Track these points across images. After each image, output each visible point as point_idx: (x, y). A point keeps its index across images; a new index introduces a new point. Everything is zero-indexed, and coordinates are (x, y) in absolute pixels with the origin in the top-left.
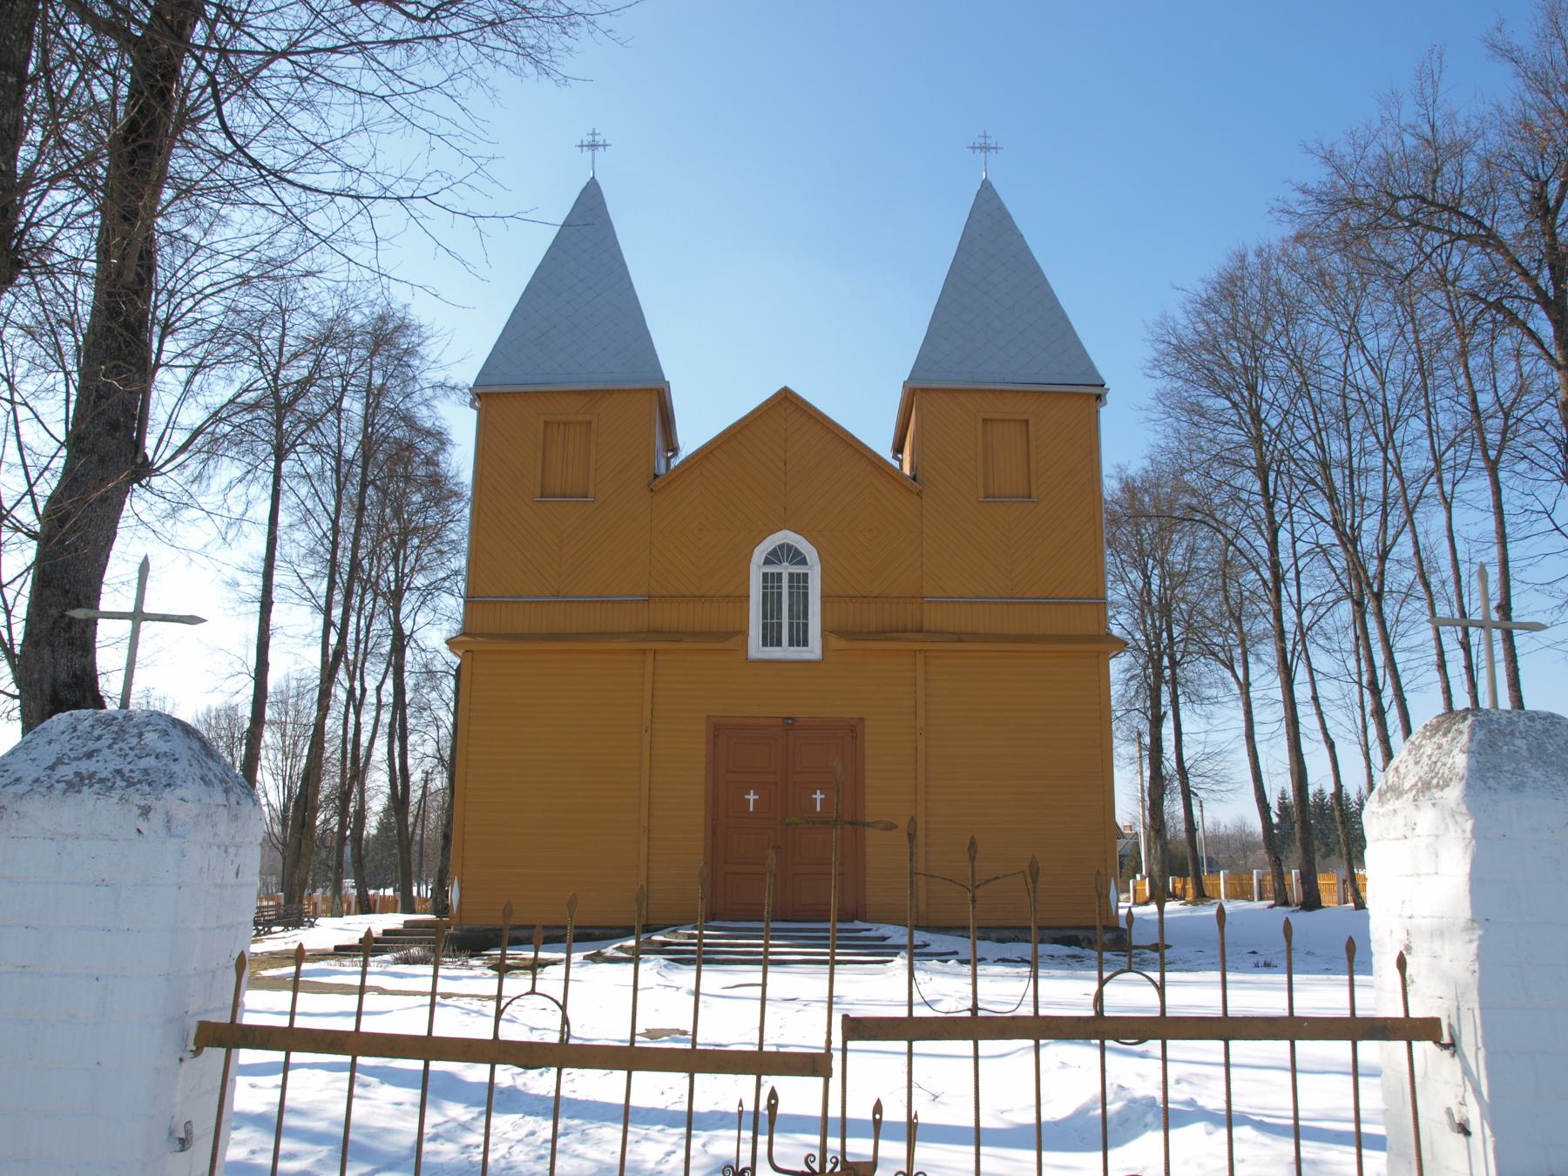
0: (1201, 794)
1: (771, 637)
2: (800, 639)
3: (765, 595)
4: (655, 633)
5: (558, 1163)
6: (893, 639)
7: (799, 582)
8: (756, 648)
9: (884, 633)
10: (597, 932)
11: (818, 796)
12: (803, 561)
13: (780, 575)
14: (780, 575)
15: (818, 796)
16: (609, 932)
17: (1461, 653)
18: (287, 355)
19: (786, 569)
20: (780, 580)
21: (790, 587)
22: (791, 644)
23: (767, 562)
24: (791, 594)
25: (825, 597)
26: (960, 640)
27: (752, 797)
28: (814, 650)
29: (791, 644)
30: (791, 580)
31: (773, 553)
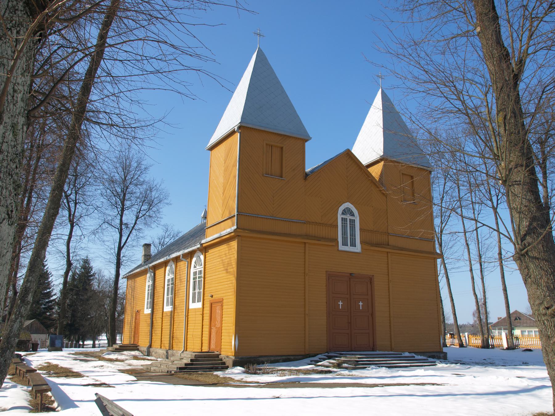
0: (114, 254)
1: (345, 244)
2: (353, 244)
3: (342, 226)
4: (308, 236)
5: (113, 272)
6: (384, 248)
7: (352, 222)
8: (341, 247)
9: (377, 245)
10: (292, 357)
11: (361, 304)
12: (353, 215)
13: (346, 219)
14: (346, 219)
15: (361, 304)
16: (296, 357)
17: (479, 265)
18: (116, 34)
19: (348, 217)
20: (347, 221)
21: (350, 224)
22: (351, 246)
23: (343, 214)
24: (350, 227)
25: (361, 229)
26: (402, 250)
27: (340, 303)
28: (358, 248)
29: (351, 246)
30: (350, 222)
31: (344, 210)
